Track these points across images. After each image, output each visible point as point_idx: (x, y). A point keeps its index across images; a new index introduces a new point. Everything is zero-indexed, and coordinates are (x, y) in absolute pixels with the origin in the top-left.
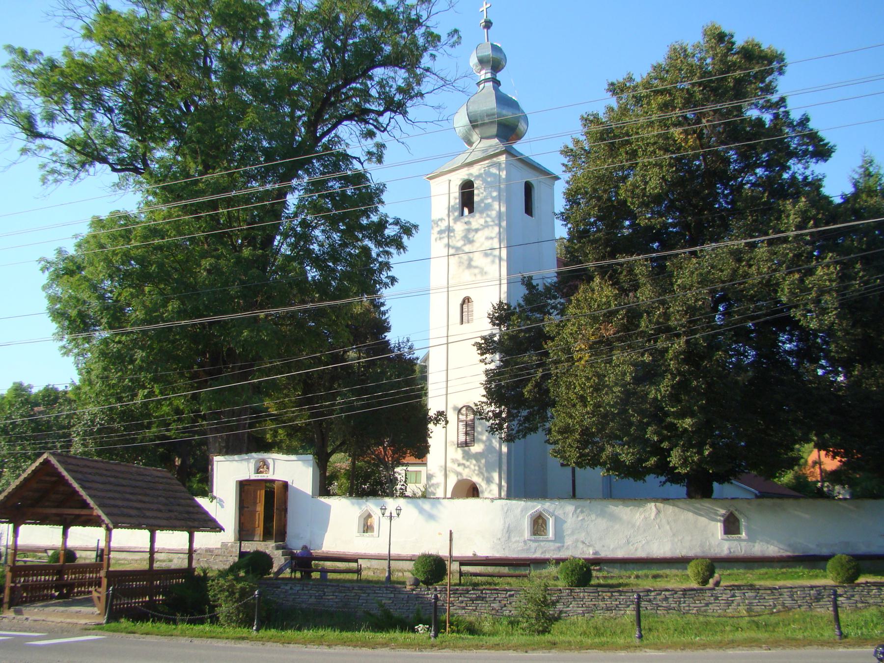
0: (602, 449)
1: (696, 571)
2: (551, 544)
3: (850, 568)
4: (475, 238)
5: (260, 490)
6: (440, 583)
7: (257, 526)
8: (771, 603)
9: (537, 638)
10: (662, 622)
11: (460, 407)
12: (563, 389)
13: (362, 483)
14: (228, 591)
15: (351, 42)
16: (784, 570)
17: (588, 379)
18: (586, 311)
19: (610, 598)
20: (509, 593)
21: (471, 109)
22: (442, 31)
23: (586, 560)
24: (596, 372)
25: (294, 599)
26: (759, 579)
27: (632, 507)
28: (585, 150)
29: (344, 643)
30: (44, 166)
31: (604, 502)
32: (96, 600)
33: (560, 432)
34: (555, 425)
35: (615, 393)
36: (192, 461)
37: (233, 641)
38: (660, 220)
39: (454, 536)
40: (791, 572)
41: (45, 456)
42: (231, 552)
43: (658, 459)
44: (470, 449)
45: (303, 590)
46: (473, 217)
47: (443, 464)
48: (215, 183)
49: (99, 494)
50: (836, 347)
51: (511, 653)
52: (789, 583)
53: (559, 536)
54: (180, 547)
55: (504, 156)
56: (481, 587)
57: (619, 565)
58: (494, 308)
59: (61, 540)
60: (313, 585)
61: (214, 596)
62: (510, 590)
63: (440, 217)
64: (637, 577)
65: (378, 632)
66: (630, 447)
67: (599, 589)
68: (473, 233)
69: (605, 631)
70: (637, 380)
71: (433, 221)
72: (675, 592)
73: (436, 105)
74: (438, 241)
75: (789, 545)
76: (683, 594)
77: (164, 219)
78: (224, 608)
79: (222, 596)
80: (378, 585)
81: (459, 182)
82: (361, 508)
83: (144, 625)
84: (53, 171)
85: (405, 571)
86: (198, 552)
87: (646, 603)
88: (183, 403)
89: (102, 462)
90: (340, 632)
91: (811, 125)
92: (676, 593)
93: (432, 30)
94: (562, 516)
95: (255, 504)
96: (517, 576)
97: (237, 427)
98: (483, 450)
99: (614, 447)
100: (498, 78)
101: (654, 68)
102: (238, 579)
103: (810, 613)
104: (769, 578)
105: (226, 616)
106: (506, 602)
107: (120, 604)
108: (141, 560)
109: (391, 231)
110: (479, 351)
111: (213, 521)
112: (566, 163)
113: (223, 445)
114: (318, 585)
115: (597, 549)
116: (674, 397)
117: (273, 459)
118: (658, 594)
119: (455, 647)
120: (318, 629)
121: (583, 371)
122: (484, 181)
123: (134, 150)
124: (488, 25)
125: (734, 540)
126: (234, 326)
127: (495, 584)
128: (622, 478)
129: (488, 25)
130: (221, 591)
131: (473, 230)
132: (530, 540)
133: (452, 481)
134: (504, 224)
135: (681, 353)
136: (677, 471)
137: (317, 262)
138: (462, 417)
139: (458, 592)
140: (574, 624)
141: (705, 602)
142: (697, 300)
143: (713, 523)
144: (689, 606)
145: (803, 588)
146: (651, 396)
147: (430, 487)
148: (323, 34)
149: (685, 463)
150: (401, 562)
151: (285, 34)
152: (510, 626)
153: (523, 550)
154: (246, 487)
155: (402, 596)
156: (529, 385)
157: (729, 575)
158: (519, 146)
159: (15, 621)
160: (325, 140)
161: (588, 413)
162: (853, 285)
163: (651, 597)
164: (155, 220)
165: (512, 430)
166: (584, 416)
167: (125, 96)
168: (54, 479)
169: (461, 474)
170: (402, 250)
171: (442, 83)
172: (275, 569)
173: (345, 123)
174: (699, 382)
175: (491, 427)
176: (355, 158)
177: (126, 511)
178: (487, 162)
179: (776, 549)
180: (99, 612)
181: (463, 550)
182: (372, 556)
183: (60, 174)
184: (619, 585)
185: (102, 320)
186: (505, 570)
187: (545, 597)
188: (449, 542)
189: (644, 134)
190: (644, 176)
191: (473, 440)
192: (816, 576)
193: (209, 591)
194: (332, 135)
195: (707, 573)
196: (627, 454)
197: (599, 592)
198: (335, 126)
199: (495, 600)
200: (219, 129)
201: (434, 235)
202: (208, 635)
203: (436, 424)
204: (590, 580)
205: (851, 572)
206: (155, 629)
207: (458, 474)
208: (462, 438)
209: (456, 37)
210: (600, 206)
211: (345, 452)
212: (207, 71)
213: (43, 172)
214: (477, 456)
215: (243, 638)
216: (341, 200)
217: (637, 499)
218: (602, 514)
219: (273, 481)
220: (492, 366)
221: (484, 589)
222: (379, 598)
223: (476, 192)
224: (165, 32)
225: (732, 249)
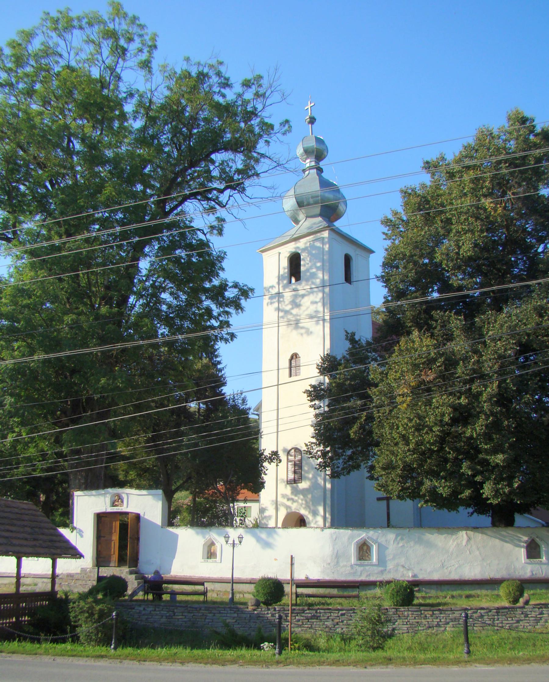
0: (421, 483)
1: (507, 591)
2: (375, 568)
4: (302, 302)
5: (115, 521)
6: (278, 603)
7: (112, 553)
9: (373, 654)
10: (479, 637)
11: (289, 448)
13: (201, 517)
14: (88, 612)
15: (195, 131)
19: (431, 616)
20: (341, 612)
21: (299, 191)
22: (275, 121)
24: (418, 414)
25: (147, 619)
27: (446, 535)
28: (403, 221)
29: (196, 660)
33: (383, 469)
35: (434, 432)
36: (55, 497)
37: (93, 659)
42: (89, 577)
43: (472, 491)
44: (297, 486)
45: (155, 610)
46: (300, 284)
47: (274, 499)
51: (352, 669)
53: (382, 561)
54: (44, 573)
55: (327, 232)
56: (316, 607)
57: (435, 586)
61: (75, 617)
63: (271, 285)
64: (453, 597)
65: (225, 649)
66: (446, 481)
67: (422, 608)
68: (300, 299)
69: (429, 646)
70: (454, 421)
71: (265, 288)
72: (489, 610)
73: (269, 185)
74: (270, 306)
76: (497, 612)
77: (32, 279)
79: (82, 617)
80: (222, 606)
82: (204, 537)
83: (11, 644)
85: (245, 593)
86: (60, 577)
88: (47, 445)
90: (191, 650)
92: (490, 611)
93: (266, 120)
94: (384, 543)
95: (111, 533)
97: (96, 462)
98: (310, 486)
99: (431, 481)
101: (465, 147)
102: (97, 602)
105: (86, 635)
106: (338, 621)
108: (9, 584)
109: (230, 293)
110: (309, 398)
112: (386, 232)
113: (82, 481)
114: (169, 606)
116: (487, 437)
117: (127, 494)
118: (474, 613)
119: (299, 663)
120: (171, 647)
121: (404, 413)
122: (310, 253)
124: (312, 121)
125: (536, 564)
126: (93, 375)
127: (328, 604)
129: (312, 121)
130: (82, 612)
132: (356, 565)
135: (492, 396)
136: (489, 502)
137: (168, 321)
139: (295, 611)
141: (516, 619)
142: (506, 350)
143: (517, 549)
144: (502, 623)
147: (263, 519)
148: (171, 125)
150: (241, 585)
151: (138, 124)
152: (343, 642)
154: (103, 519)
155: (244, 616)
156: (355, 427)
158: (338, 224)
164: (23, 281)
170: (240, 310)
171: (275, 164)
172: (129, 592)
176: (199, 230)
178: (312, 236)
181: (300, 575)
182: (216, 579)
184: (439, 604)
186: (335, 591)
187: (379, 616)
188: (290, 566)
189: (457, 203)
190: (457, 241)
193: (70, 613)
194: (179, 209)
195: (517, 593)
196: (444, 488)
197: (421, 611)
198: (181, 203)
199: (328, 618)
200: (81, 201)
202: (70, 653)
204: (413, 600)
206: (21, 648)
207: (287, 507)
208: (291, 476)
209: (287, 127)
210: (416, 270)
211: (187, 490)
212: (69, 152)
214: (304, 492)
215: (102, 657)
218: (420, 541)
219: (127, 513)
220: (321, 410)
221: (319, 609)
222: (224, 618)
223: (302, 263)
224: (33, 117)
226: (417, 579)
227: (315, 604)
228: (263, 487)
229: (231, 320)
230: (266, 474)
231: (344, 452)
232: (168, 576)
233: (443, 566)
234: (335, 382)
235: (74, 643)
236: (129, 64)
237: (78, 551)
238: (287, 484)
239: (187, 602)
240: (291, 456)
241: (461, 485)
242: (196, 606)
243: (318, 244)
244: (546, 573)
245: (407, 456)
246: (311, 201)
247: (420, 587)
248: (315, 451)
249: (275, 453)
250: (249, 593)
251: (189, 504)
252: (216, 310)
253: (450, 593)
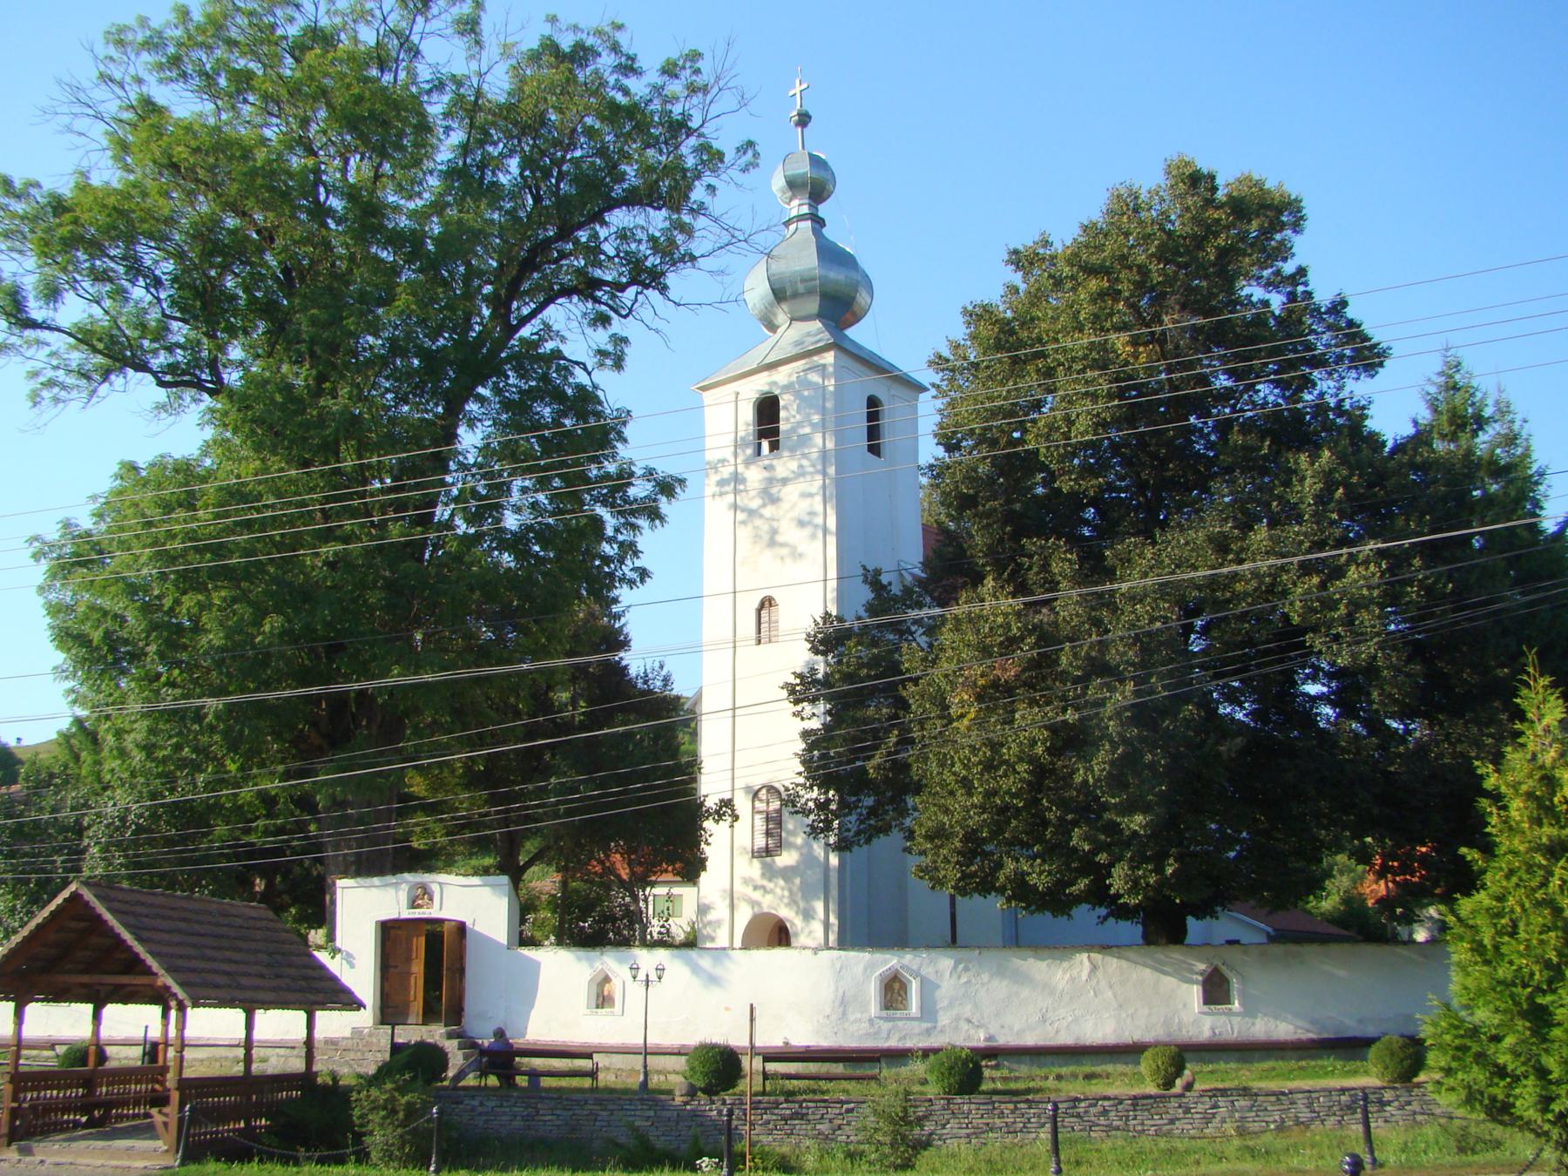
0: (1000, 865)
1: (1154, 1067)
2: (915, 1023)
3: (1406, 1058)
4: (782, 495)
5: (418, 936)
6: (731, 1091)
7: (412, 998)
8: (1277, 1118)
11: (757, 788)
12: (934, 767)
16: (1303, 1063)
17: (973, 749)
18: (971, 637)
19: (1013, 1112)
23: (974, 1050)
25: (486, 1121)
26: (1261, 1079)
30: (35, 374)
31: (1007, 953)
32: (160, 1128)
34: (921, 825)
38: (1094, 482)
39: (757, 1013)
40: (1314, 1067)
41: (73, 887)
43: (1091, 881)
44: (774, 861)
45: (501, 1106)
47: (728, 886)
48: (342, 413)
49: (165, 949)
50: (1380, 695)
52: (1307, 1084)
55: (832, 353)
56: (800, 1098)
58: (817, 624)
60: (519, 1097)
61: (362, 1117)
62: (848, 1102)
64: (1059, 1077)
66: (1044, 861)
67: (995, 1098)
69: (1005, 1166)
71: (708, 463)
75: (1313, 1022)
76: (1132, 1104)
77: (256, 475)
78: (377, 1138)
79: (376, 1117)
81: (754, 396)
82: (592, 967)
83: (245, 1168)
84: (51, 383)
87: (1072, 1119)
89: (163, 895)
91: (1350, 313)
94: (932, 977)
95: (409, 960)
96: (858, 1079)
99: (1018, 861)
100: (820, 215)
101: (1085, 228)
103: (1339, 1133)
104: (1277, 1076)
107: (200, 1135)
109: (639, 490)
111: (346, 992)
115: (992, 1031)
116: (1116, 780)
120: (536, 1168)
122: (797, 394)
123: (192, 346)
124: (804, 120)
125: (1221, 1014)
127: (823, 1093)
128: (1032, 913)
129: (804, 120)
131: (778, 481)
133: (744, 916)
134: (832, 470)
135: (1126, 709)
136: (1122, 901)
138: (760, 806)
139: (762, 1106)
140: (953, 1156)
141: (1169, 1116)
142: (1152, 620)
143: (1185, 986)
144: (1142, 1124)
145: (1329, 1091)
146: (1078, 779)
149: (1135, 886)
150: (662, 1057)
152: (848, 1160)
153: (868, 1034)
155: (668, 1114)
157: (1212, 1072)
159: (22, 1165)
160: (526, 332)
161: (974, 806)
162: (1408, 593)
163: (1082, 1110)
165: (849, 830)
166: (968, 811)
167: (180, 256)
168: (83, 924)
169: (759, 904)
170: (657, 522)
171: (726, 238)
172: (451, 1073)
173: (560, 301)
174: (1156, 755)
175: (812, 826)
176: (578, 363)
177: (209, 977)
178: (803, 362)
179: (1291, 1028)
181: (769, 1038)
183: (64, 387)
184: (1028, 1091)
185: (149, 649)
186: (838, 1068)
191: (780, 845)
192: (1355, 1073)
197: (994, 1102)
198: (542, 307)
199: (822, 1118)
200: (350, 320)
201: (711, 487)
203: (717, 822)
205: (1406, 1063)
207: (754, 903)
208: (761, 842)
209: (750, 153)
212: (320, 212)
213: (34, 384)
214: (787, 873)
216: (559, 443)
217: (1058, 947)
218: (1001, 972)
219: (440, 921)
220: (815, 724)
221: (805, 1100)
222: (631, 1119)
223: (782, 414)
225: (1213, 533)
226: (995, 1044)
227: (801, 1092)
228: (704, 869)
229: (642, 542)
230: (709, 844)
231: (859, 801)
232: (521, 1041)
233: (1044, 1019)
234: (839, 671)
235: (361, 1164)
236: (435, 25)
237: (355, 997)
238: (753, 857)
239: (559, 1090)
240: (761, 800)
241: (1069, 869)
242: (578, 1096)
243: (815, 378)
244: (1239, 1032)
245: (970, 817)
246: (801, 288)
247: (1000, 1059)
248: (803, 801)
249: (727, 803)
250: (678, 1073)
251: (554, 892)
252: (610, 521)
253: (1056, 1070)
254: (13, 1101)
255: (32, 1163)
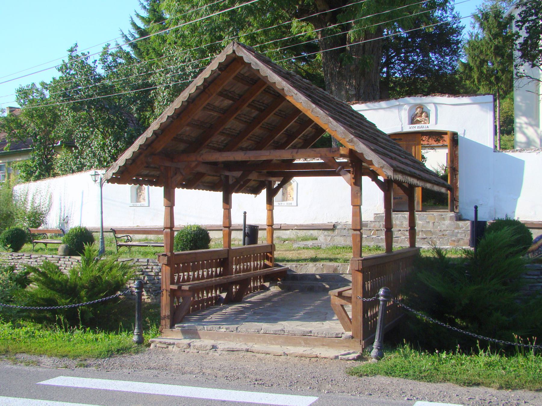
54: (325, 222)
59: (349, 209)
117: (435, 104)
159: (192, 350)
180: (350, 333)
254: (172, 283)
255: (203, 348)
